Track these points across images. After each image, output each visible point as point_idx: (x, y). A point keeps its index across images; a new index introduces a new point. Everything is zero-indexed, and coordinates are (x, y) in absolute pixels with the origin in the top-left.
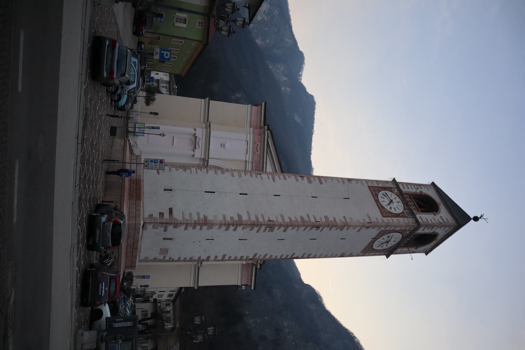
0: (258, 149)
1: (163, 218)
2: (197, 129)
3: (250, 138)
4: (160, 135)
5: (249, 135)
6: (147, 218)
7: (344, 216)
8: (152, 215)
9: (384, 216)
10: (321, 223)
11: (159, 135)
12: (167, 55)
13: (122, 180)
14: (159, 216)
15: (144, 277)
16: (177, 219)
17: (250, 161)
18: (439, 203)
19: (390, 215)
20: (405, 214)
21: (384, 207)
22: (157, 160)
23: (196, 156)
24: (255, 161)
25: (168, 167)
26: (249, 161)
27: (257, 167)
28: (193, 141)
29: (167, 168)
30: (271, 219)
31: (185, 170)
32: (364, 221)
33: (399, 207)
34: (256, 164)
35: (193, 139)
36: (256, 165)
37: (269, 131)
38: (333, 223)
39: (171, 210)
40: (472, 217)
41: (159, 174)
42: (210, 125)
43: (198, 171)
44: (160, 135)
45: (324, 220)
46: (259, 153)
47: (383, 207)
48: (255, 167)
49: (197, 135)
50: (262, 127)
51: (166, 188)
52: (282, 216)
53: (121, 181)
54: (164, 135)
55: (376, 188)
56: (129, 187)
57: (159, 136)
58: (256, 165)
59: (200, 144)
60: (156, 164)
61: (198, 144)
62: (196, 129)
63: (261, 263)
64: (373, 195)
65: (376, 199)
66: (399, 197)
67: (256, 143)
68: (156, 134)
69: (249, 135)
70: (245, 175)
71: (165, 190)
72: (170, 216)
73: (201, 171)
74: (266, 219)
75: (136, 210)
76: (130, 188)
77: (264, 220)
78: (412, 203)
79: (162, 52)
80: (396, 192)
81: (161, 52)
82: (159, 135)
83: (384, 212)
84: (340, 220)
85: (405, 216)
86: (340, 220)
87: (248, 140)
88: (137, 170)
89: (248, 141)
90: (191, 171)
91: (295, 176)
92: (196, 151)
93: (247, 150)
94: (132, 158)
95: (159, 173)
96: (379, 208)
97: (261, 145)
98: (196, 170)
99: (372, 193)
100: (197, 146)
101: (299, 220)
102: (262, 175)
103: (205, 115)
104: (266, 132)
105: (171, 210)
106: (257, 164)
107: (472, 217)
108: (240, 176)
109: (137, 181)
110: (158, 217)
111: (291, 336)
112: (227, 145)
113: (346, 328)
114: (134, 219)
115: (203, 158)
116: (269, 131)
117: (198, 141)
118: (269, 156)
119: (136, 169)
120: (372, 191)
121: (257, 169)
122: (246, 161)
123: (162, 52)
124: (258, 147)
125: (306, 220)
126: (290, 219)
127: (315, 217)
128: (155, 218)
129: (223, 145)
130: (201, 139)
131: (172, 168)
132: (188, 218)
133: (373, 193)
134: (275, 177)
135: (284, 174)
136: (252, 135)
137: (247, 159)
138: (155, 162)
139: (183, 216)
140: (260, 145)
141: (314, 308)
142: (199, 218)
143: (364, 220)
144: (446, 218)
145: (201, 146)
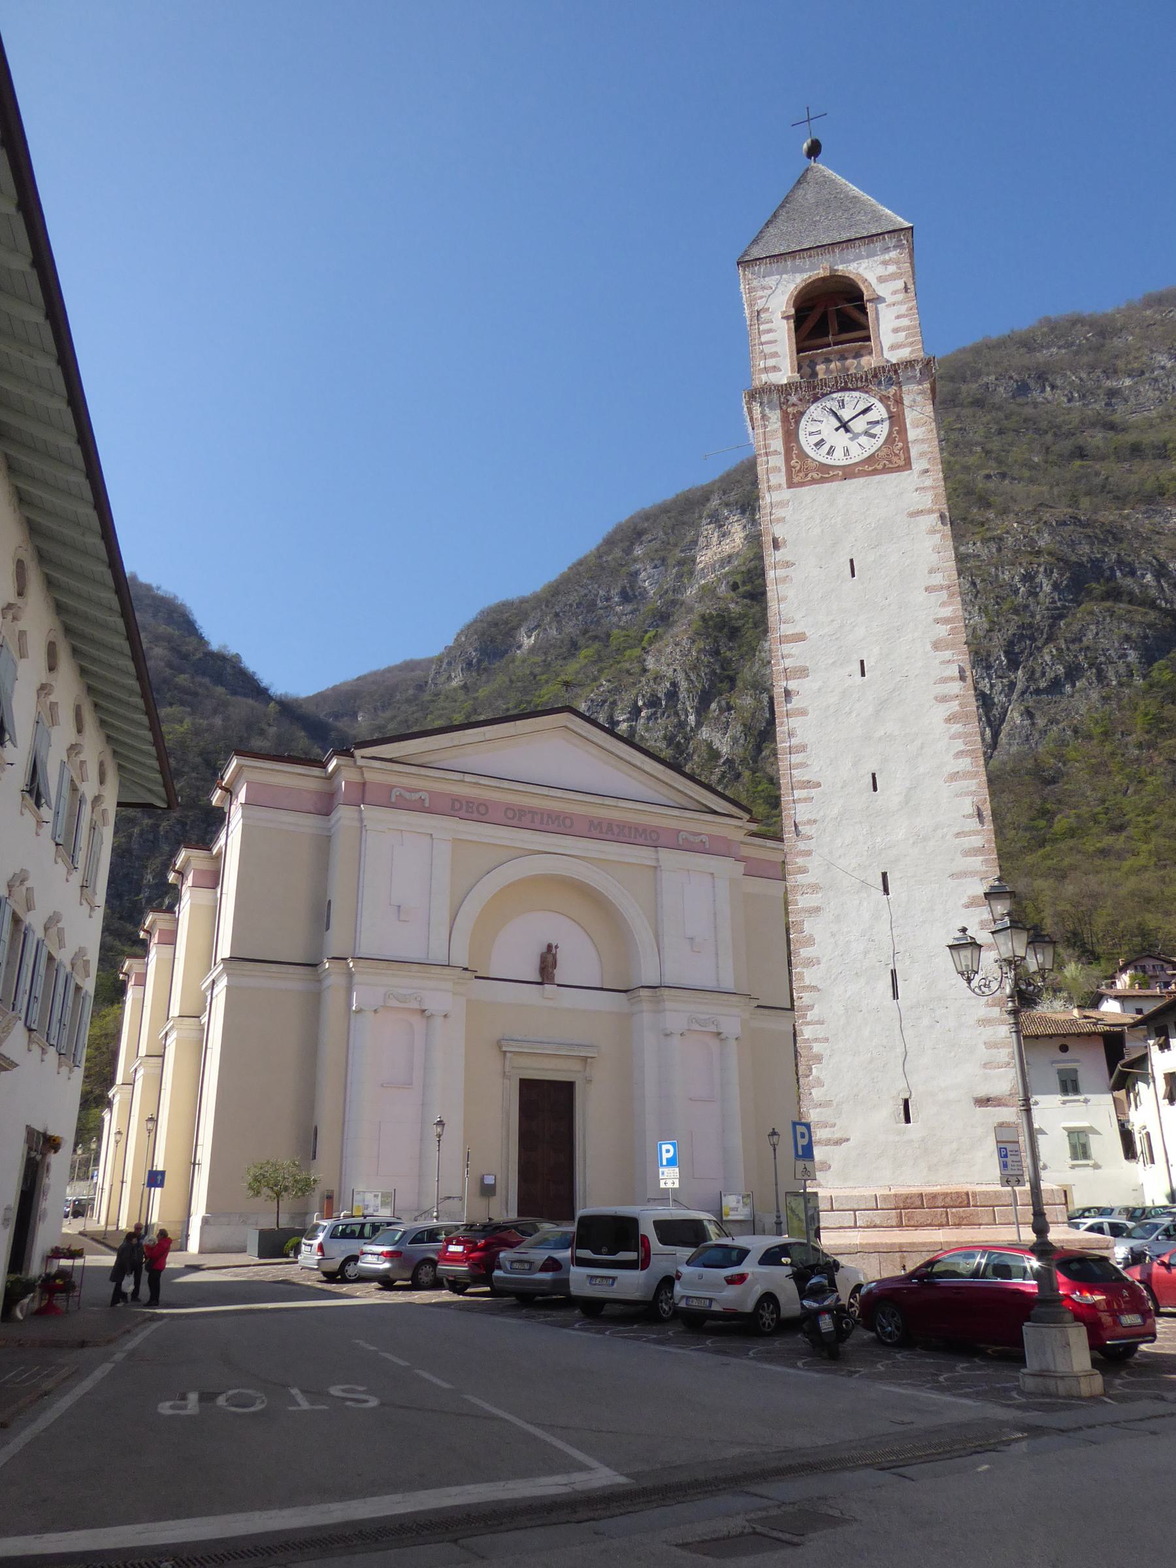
4: (774, 1146)
7: (923, 588)
9: (905, 464)
11: (775, 1150)
15: (800, 1153)
19: (901, 444)
21: (869, 457)
22: (1001, 1148)
27: (471, 805)
38: (956, 627)
39: (984, 1102)
41: (848, 1140)
45: (947, 655)
47: (871, 459)
48: (472, 812)
51: (902, 1116)
54: (774, 1133)
57: (777, 1147)
58: (464, 807)
60: (1009, 1153)
64: (823, 480)
68: (775, 1158)
71: (908, 1120)
72: (1006, 1105)
79: (665, 1163)
82: (775, 1150)
83: (890, 462)
84: (943, 604)
88: (856, 1207)
90: (816, 1040)
96: (875, 472)
98: (808, 1024)
99: (814, 481)
105: (984, 1102)
119: (850, 1210)
123: (665, 1163)
126: (959, 754)
127: (945, 680)
133: (815, 476)
138: (1006, 1156)
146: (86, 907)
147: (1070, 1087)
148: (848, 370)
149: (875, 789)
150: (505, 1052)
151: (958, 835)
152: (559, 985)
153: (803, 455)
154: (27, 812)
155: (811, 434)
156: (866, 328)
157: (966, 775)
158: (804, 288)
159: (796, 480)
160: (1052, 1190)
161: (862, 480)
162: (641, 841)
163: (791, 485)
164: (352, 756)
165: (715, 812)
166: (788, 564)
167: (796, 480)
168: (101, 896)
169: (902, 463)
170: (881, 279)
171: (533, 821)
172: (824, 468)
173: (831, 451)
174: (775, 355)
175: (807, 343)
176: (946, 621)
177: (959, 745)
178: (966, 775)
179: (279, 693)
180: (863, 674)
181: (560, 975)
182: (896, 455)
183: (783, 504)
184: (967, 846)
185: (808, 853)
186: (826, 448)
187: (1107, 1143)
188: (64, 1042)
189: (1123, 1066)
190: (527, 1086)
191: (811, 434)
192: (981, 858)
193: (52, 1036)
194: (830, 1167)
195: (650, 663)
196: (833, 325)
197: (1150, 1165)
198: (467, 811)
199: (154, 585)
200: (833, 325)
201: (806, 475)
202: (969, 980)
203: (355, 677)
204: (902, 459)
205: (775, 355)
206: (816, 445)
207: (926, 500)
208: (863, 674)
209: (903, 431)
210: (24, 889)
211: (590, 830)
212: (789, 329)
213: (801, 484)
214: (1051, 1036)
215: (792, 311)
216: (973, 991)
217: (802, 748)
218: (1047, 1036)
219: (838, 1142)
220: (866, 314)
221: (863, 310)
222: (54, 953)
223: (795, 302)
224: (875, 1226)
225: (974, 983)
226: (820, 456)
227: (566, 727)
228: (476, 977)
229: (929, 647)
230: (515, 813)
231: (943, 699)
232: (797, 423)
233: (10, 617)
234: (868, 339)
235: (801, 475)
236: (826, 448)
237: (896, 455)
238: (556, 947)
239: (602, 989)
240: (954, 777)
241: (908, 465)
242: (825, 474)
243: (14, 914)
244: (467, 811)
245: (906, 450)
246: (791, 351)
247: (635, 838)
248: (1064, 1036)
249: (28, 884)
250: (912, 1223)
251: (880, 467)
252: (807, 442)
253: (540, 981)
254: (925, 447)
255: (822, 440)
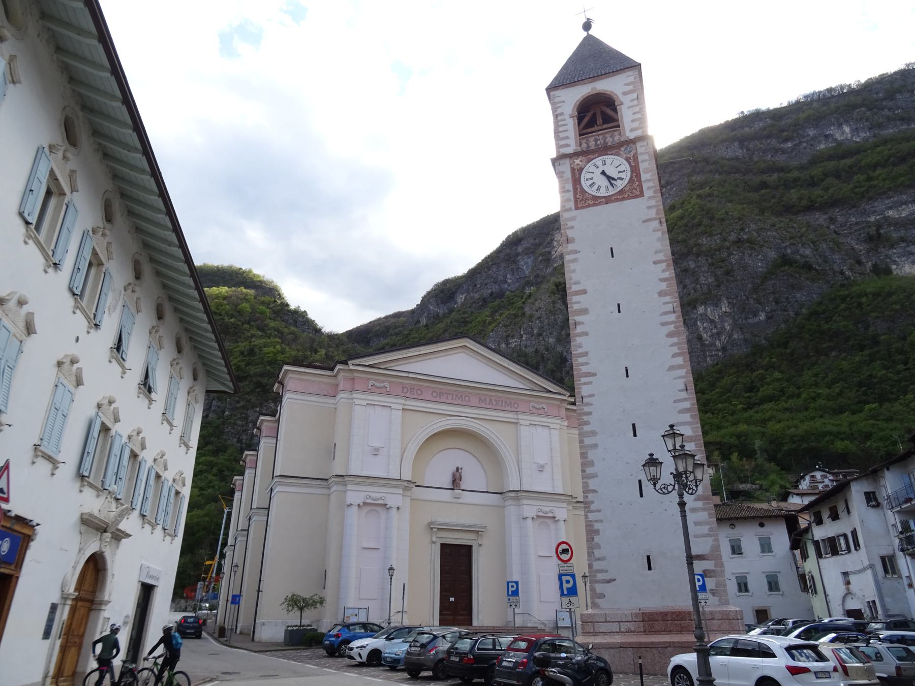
0: (382, 385)
1: (714, 571)
2: (349, 501)
3: (360, 399)
5: (357, 402)
6: (719, 599)
8: (712, 590)
10: (675, 304)
11: (391, 579)
12: (568, 582)
13: (667, 647)
14: (710, 577)
16: (711, 547)
17: (403, 401)
18: (592, 89)
19: (637, 183)
20: (628, 155)
23: (399, 504)
24: (403, 392)
25: (595, 563)
26: (404, 405)
28: (371, 510)
29: (597, 565)
30: (683, 387)
31: (597, 532)
32: (658, 230)
33: (617, 163)
34: (407, 392)
35: (366, 509)
36: (409, 392)
37: (349, 362)
40: (585, 34)
42: (336, 475)
43: (593, 507)
44: (391, 576)
46: (387, 385)
48: (413, 394)
49: (360, 502)
50: (332, 374)
52: (672, 368)
53: (669, 648)
54: (391, 569)
55: (578, 196)
56: (663, 633)
58: (409, 392)
59: (378, 495)
61: (378, 500)
62: (349, 503)
63: (569, 394)
64: (595, 205)
65: (604, 200)
66: (593, 159)
67: (370, 388)
69: (357, 402)
70: (590, 424)
71: (650, 568)
73: (592, 502)
74: (684, 395)
75: (713, 619)
76: (664, 631)
77: (685, 400)
78: (601, 137)
80: (581, 161)
81: (565, 595)
82: (391, 579)
83: (632, 193)
84: (664, 271)
85: (634, 156)
86: (664, 271)
87: (365, 403)
88: (619, 620)
89: (367, 404)
90: (596, 521)
91: (576, 336)
92: (389, 504)
93: (382, 406)
94: (592, 630)
95: (611, 579)
96: (623, 199)
97: (375, 380)
99: (589, 206)
100: (550, 515)
101: (675, 340)
102: (583, 394)
103: (292, 485)
104: (352, 367)
106: (408, 390)
107: (585, 34)
108: (593, 433)
109: (646, 619)
110: (714, 579)
111: (513, 340)
112: (376, 445)
113: (500, 247)
114: (734, 621)
115: (402, 490)
116: (349, 362)
117: (372, 499)
118: (395, 366)
120: (587, 204)
121: (416, 389)
122: (403, 409)
124: (377, 384)
125: (673, 329)
128: (716, 584)
129: (376, 452)
130: (367, 493)
131: (594, 556)
132: (707, 527)
133: (591, 203)
134: (583, 371)
135: (575, 354)
136: (355, 396)
137: (401, 407)
139: (703, 536)
140: (374, 382)
141: (463, 296)
142: (704, 509)
143: (655, 230)
144: (625, 85)
145: (382, 495)
146: (183, 448)
147: (766, 548)
148: (607, 143)
149: (627, 376)
150: (432, 528)
151: (675, 401)
152: (463, 490)
153: (583, 192)
154: (141, 396)
155: (587, 180)
156: (618, 121)
157: (680, 367)
158: (582, 100)
159: (579, 205)
160: (736, 611)
161: (616, 204)
162: (509, 409)
163: (577, 208)
164: (347, 364)
165: (550, 392)
166: (576, 252)
167: (579, 205)
168: (194, 441)
169: (638, 193)
170: (625, 93)
171: (447, 398)
172: (595, 198)
173: (599, 189)
174: (567, 138)
175: (585, 131)
176: (664, 280)
177: (675, 350)
178: (680, 367)
179: (327, 331)
180: (619, 311)
181: (464, 485)
182: (635, 189)
183: (573, 219)
184: (680, 408)
185: (590, 413)
186: (596, 187)
187: (788, 582)
188: (169, 522)
189: (795, 535)
190: (444, 546)
191: (587, 180)
192: (689, 414)
193: (158, 519)
194: (604, 596)
195: (527, 310)
196: (600, 120)
197: (815, 595)
198: (411, 393)
199: (261, 275)
200: (600, 120)
201: (585, 202)
202: (655, 485)
203: (368, 322)
204: (638, 190)
205: (567, 138)
206: (590, 186)
207: (653, 213)
208: (619, 311)
209: (638, 176)
210: (140, 438)
211: (479, 403)
212: (574, 124)
213: (582, 208)
214: (753, 518)
215: (576, 114)
216: (657, 491)
217: (586, 354)
218: (751, 517)
219: (609, 581)
220: (617, 113)
221: (615, 110)
222: (161, 473)
223: (577, 108)
224: (631, 632)
225: (658, 486)
226: (592, 191)
227: (465, 346)
228: (416, 486)
229: (656, 296)
230: (408, 390)
231: (664, 324)
232: (580, 175)
233: (130, 291)
234: (618, 126)
235: (582, 202)
236: (596, 187)
237: (635, 189)
238: (461, 469)
239: (487, 492)
240: (672, 368)
241: (642, 194)
242: (597, 201)
243: (132, 451)
244: (411, 393)
245: (641, 186)
246: (575, 135)
247: (456, 400)
248: (762, 517)
249: (141, 435)
250: (653, 630)
251: (626, 196)
252: (585, 184)
253: (452, 487)
254: (651, 184)
255: (594, 183)
